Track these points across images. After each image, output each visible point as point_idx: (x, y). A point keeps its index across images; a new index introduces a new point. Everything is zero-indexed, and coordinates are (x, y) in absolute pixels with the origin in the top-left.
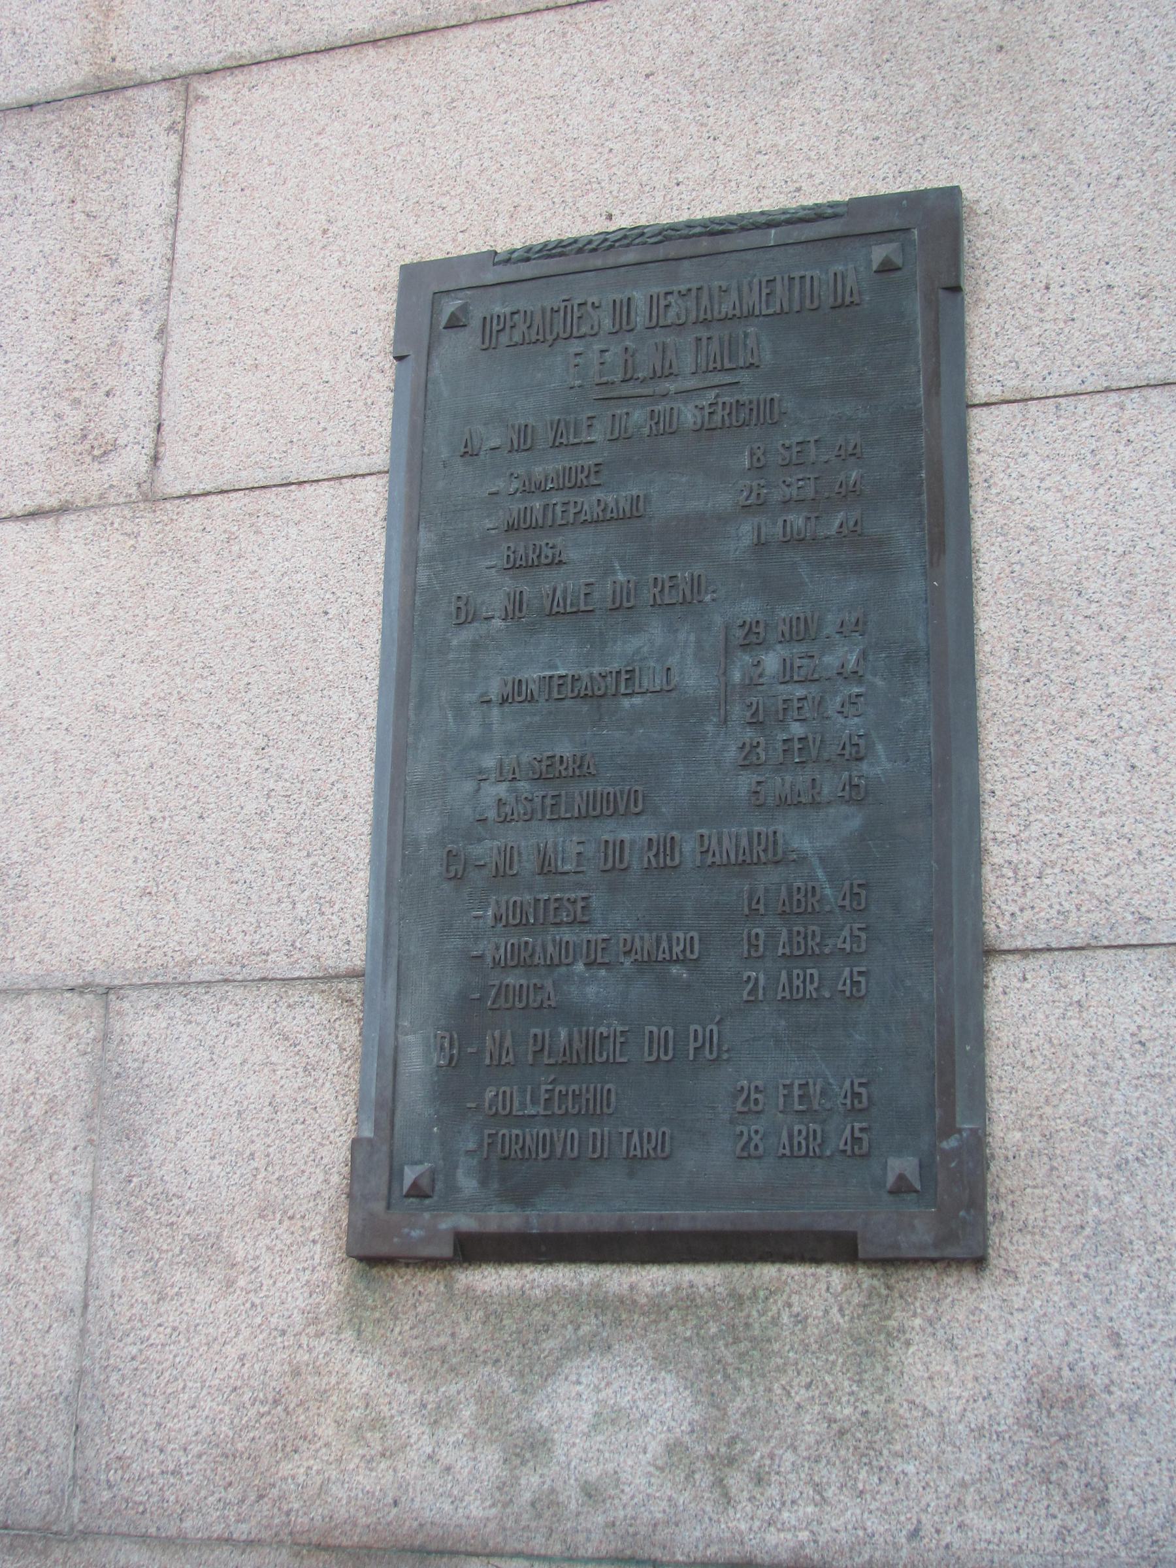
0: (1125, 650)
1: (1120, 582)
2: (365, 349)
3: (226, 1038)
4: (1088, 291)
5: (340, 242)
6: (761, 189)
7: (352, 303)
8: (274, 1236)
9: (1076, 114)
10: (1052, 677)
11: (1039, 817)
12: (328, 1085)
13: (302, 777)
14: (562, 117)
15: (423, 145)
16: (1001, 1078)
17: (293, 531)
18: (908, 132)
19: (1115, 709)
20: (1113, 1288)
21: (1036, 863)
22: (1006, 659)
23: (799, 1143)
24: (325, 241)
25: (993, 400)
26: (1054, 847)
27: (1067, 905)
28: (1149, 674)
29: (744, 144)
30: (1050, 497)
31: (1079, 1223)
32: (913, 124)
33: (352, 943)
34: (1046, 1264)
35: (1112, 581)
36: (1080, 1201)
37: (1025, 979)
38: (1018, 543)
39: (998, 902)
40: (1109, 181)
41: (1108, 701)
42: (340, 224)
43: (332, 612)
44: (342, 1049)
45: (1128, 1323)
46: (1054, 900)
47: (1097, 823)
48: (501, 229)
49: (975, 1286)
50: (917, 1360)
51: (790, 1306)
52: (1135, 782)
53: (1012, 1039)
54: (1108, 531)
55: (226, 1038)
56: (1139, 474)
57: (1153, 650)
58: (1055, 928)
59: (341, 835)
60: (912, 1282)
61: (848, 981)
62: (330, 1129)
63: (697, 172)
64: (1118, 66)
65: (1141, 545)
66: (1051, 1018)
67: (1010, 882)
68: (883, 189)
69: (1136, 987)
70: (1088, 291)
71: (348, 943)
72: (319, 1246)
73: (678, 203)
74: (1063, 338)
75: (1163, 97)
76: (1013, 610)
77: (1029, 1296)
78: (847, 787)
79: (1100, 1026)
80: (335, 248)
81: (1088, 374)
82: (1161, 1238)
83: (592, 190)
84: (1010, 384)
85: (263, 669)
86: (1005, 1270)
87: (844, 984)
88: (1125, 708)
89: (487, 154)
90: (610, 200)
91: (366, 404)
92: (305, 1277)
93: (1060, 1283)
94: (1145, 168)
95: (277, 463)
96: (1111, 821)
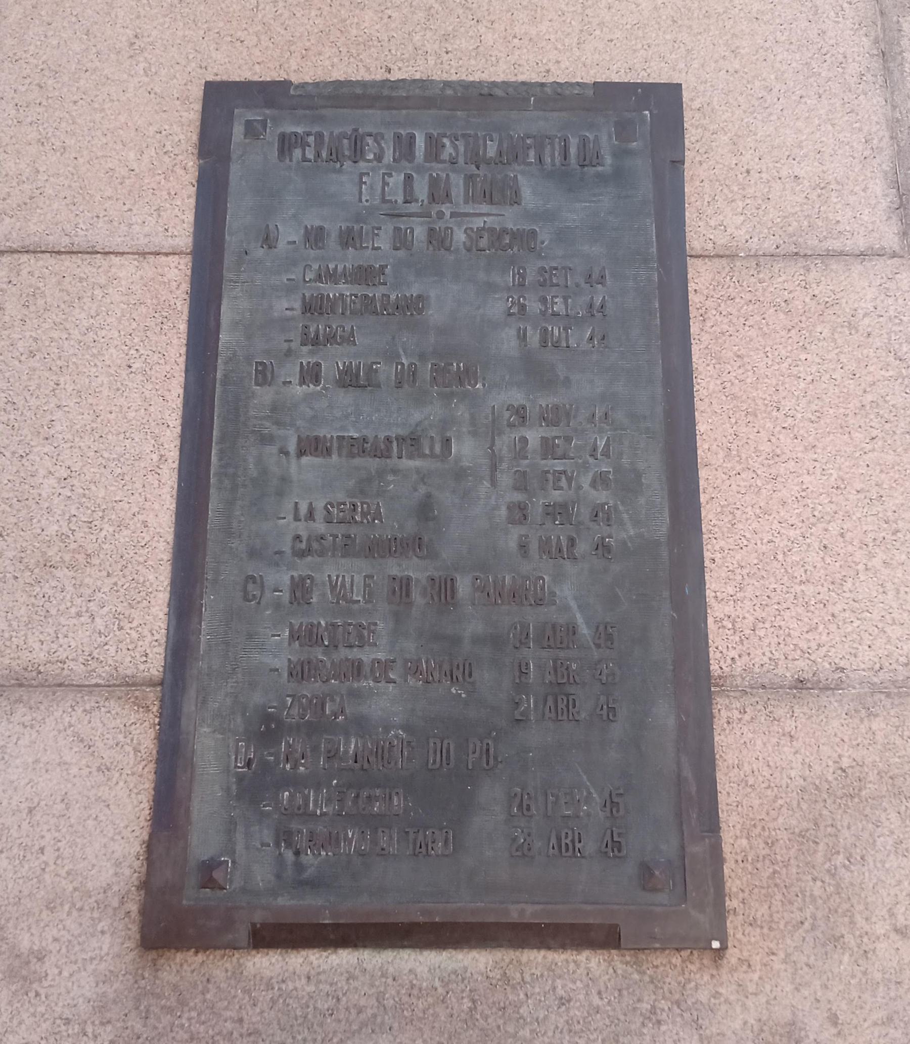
0: (816, 456)
1: (810, 402)
3: (18, 739)
8: (60, 926)
10: (759, 472)
11: (751, 582)
12: (121, 784)
13: (104, 507)
16: (728, 793)
17: (98, 292)
18: (636, 39)
19: (809, 501)
20: (830, 975)
21: (751, 619)
27: (777, 655)
28: (835, 476)
29: (503, 29)
30: (753, 333)
31: (799, 919)
32: (640, 33)
33: (150, 655)
34: (773, 954)
35: (803, 402)
36: (799, 899)
39: (720, 648)
40: (794, 98)
41: (803, 494)
42: (146, 40)
43: (136, 366)
44: (136, 750)
45: (844, 1006)
47: (798, 588)
48: (294, 65)
49: (715, 972)
50: (667, 1038)
52: (828, 560)
53: (736, 762)
54: (799, 363)
55: (18, 739)
56: (823, 322)
57: (838, 457)
59: (141, 559)
60: (662, 969)
61: (605, 707)
62: (122, 825)
63: (463, 45)
64: (798, 14)
65: (826, 377)
69: (835, 723)
70: (780, 178)
71: (146, 655)
72: (108, 936)
75: (832, 42)
78: (600, 547)
79: (808, 754)
80: (141, 59)
82: (867, 933)
83: (374, 46)
85: (66, 409)
87: (602, 709)
88: (817, 501)
90: (389, 57)
91: (169, 194)
92: (91, 968)
93: (786, 970)
94: (821, 92)
95: (83, 233)
96: (809, 590)
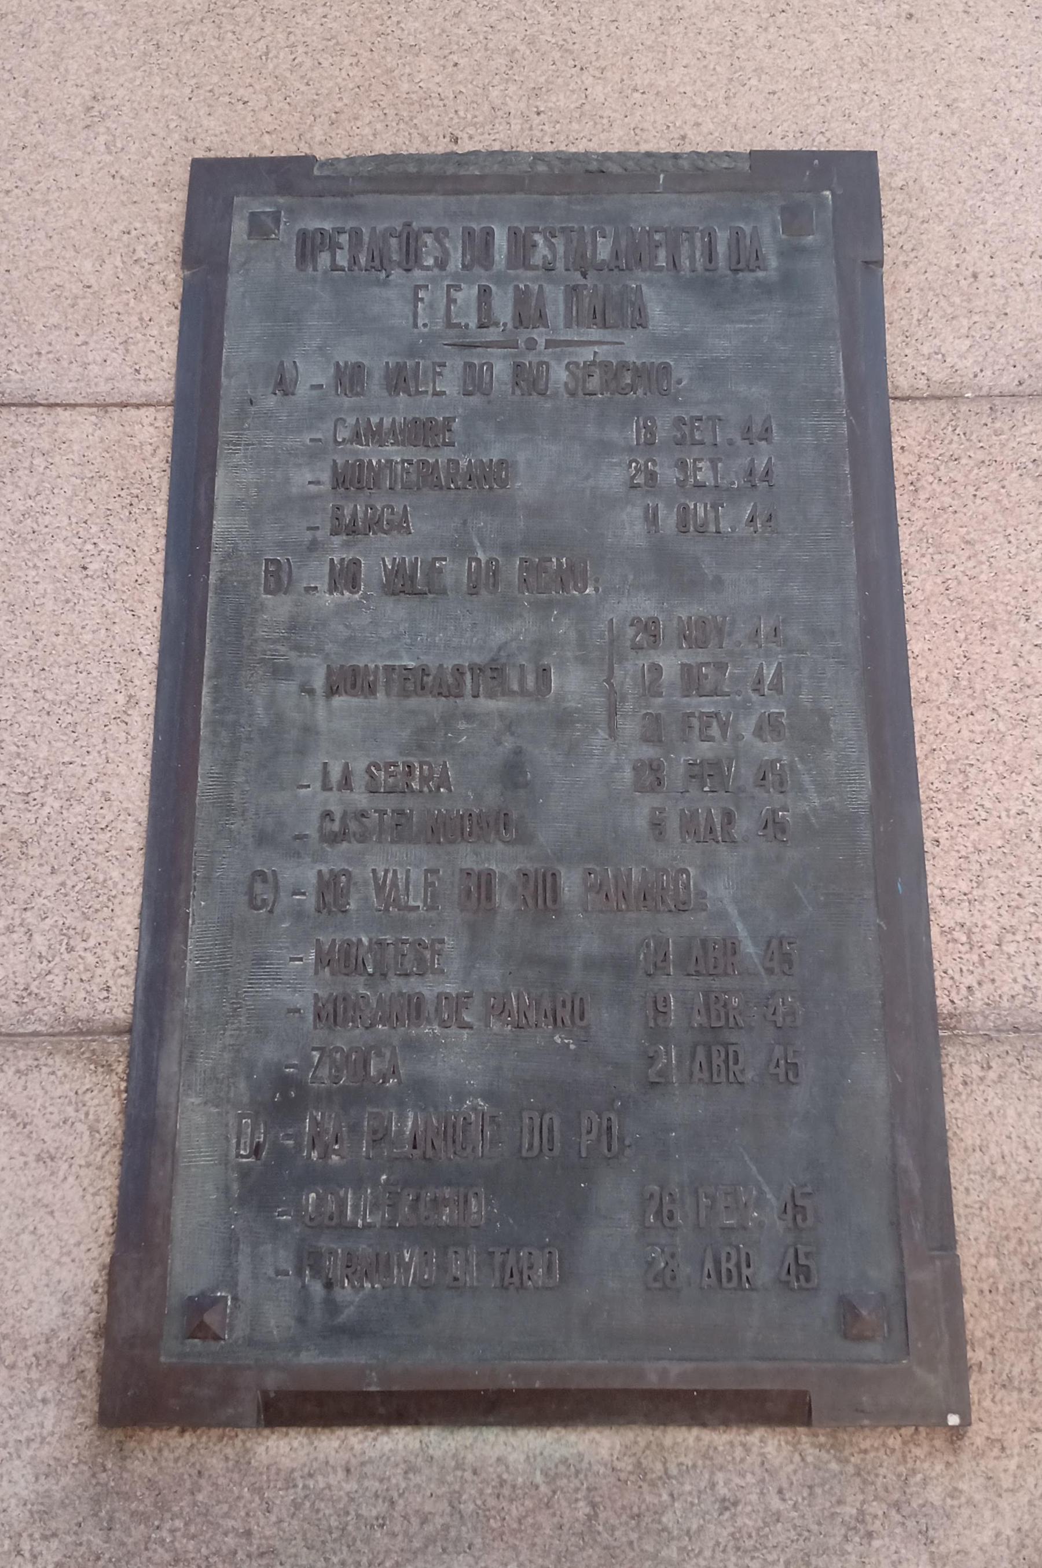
2: (141, 254)
4: (1021, 285)
5: (109, 123)
6: (638, 131)
7: (124, 198)
9: (997, 95)
10: (1002, 711)
12: (71, 1180)
13: (46, 772)
14: (395, 19)
15: (220, 28)
16: (967, 1190)
21: (995, 928)
22: (945, 687)
23: (729, 1271)
24: (88, 122)
25: (917, 394)
26: (1013, 909)
30: (987, 507)
33: (114, 989)
37: (990, 1067)
38: (953, 557)
39: (950, 972)
44: (93, 1130)
46: (1019, 974)
48: (319, 136)
49: (952, 1459)
51: (713, 1485)
58: (1022, 1007)
61: (782, 1062)
62: (72, 1241)
66: (1024, 1116)
67: (963, 949)
68: (781, 146)
70: (1021, 285)
71: (108, 989)
73: (540, 134)
74: (995, 334)
76: (949, 630)
77: (1019, 1472)
80: (102, 130)
81: (1026, 376)
83: (433, 106)
84: (936, 377)
86: (988, 1438)
87: (778, 1065)
89: (301, 49)
90: (456, 120)
